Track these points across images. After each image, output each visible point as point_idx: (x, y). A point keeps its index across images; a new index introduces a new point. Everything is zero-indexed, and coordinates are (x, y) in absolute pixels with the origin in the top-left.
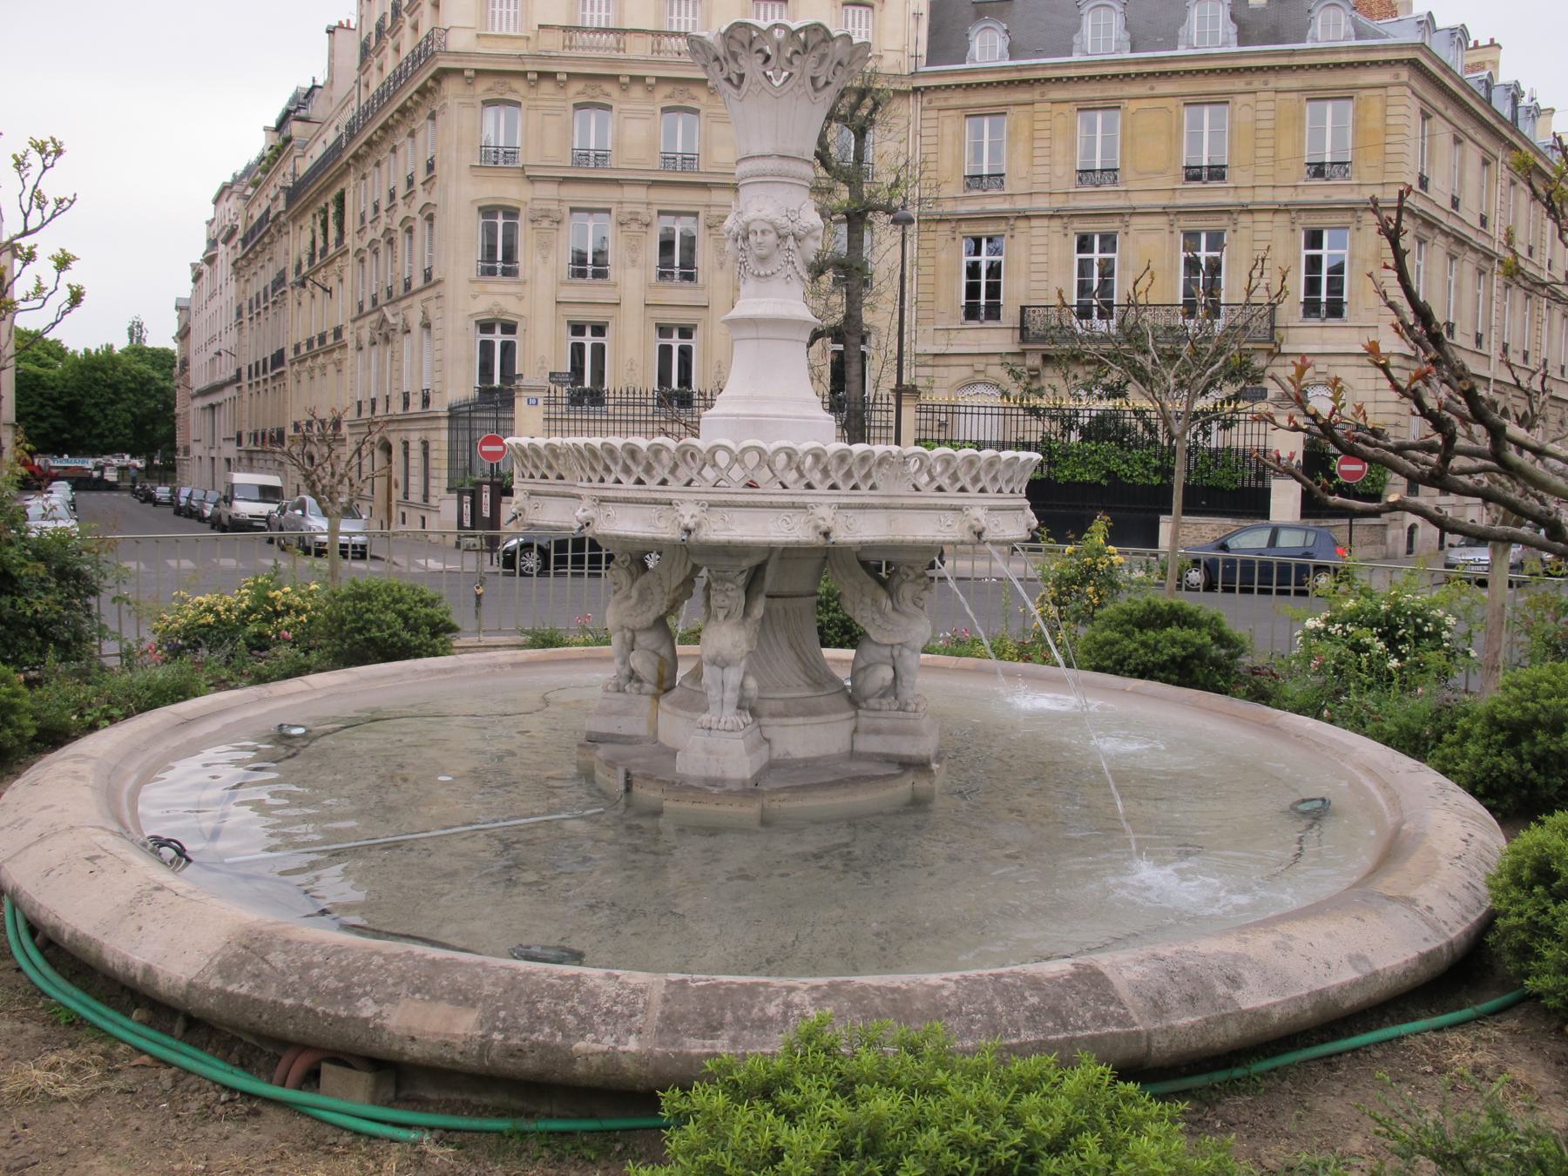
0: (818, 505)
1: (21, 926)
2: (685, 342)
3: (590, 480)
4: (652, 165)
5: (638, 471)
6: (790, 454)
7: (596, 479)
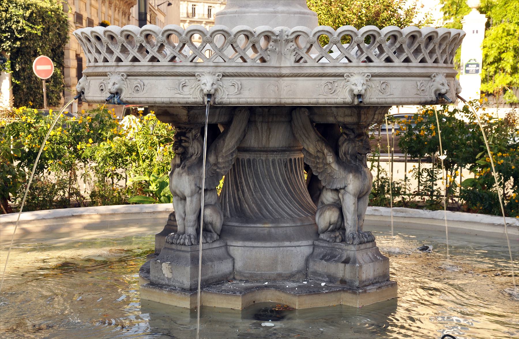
0: (351, 75)
1: (303, 165)
3: (96, 61)
4: (383, 288)
5: (134, 52)
6: (248, 35)
7: (100, 58)
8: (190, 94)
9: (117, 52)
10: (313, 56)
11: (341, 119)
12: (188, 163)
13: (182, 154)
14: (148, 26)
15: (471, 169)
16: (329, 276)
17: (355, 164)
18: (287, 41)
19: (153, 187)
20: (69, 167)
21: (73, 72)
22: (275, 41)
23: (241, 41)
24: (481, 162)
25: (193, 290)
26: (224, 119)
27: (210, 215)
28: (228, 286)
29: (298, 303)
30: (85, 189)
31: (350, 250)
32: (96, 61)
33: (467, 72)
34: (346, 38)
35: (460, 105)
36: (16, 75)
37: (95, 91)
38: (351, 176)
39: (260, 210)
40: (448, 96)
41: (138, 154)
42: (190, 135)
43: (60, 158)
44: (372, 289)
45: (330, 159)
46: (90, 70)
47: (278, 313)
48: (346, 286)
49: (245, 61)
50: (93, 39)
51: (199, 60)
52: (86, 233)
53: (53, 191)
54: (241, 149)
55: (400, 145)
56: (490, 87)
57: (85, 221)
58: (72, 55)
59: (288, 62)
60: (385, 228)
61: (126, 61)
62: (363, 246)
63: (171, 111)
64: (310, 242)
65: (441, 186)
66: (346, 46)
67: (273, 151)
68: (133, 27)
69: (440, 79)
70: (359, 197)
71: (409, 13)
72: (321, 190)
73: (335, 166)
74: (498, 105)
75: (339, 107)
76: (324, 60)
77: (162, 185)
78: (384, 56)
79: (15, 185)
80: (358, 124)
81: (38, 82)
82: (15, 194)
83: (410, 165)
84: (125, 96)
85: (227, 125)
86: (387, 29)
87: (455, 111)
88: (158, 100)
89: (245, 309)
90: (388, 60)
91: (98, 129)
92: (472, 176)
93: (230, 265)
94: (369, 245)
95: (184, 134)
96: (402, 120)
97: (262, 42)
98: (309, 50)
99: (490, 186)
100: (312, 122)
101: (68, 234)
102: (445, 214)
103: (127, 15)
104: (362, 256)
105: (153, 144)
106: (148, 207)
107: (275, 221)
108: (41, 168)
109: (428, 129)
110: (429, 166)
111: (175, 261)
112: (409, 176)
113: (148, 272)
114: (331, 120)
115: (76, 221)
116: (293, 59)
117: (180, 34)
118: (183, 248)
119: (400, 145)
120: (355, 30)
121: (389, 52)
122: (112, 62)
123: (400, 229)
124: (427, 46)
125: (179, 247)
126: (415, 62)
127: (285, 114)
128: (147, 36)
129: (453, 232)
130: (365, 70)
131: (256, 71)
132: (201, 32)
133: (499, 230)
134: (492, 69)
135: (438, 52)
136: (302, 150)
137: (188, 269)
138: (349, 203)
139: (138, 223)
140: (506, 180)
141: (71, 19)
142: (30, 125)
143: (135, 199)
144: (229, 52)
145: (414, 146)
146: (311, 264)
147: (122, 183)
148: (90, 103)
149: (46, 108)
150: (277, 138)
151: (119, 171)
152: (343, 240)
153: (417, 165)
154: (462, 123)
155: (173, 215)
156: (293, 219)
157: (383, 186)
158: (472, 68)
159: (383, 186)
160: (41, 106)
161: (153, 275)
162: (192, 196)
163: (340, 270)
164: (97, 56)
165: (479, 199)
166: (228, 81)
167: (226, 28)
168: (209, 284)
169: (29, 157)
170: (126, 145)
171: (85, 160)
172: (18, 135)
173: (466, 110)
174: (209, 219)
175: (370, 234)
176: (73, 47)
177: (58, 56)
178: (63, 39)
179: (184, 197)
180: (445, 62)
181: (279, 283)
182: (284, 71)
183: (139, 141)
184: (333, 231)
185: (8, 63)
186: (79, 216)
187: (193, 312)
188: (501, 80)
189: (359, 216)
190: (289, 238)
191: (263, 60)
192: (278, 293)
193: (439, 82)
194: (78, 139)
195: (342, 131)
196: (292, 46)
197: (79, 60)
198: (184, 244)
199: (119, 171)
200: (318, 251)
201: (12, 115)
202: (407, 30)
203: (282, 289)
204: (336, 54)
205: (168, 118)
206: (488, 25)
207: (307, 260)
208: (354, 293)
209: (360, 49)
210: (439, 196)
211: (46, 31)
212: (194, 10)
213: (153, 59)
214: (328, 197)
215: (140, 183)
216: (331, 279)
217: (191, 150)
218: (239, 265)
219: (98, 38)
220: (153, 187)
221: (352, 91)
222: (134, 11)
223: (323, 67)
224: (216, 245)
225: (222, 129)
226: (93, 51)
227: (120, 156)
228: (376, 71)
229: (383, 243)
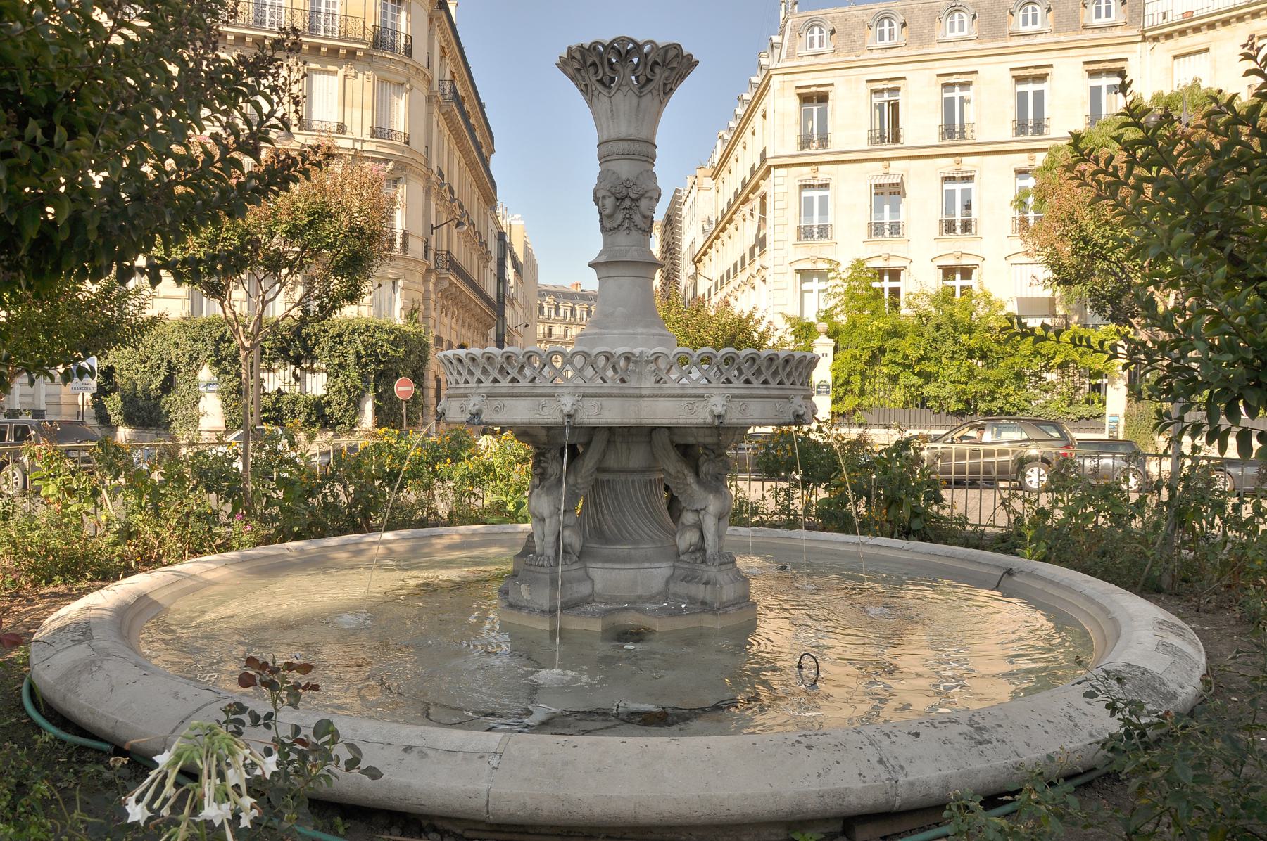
0: (711, 396)
2: (895, 284)
3: (457, 382)
5: (494, 374)
6: (608, 356)
8: (550, 414)
9: (478, 374)
10: (673, 377)
11: (701, 440)
12: (547, 484)
13: (541, 474)
14: (507, 348)
15: (826, 488)
16: (689, 598)
17: (716, 484)
18: (648, 362)
19: (510, 507)
20: (428, 487)
21: (432, 393)
22: (635, 362)
23: (601, 361)
24: (835, 481)
25: (552, 612)
26: (583, 439)
27: (568, 536)
28: (588, 608)
29: (658, 625)
30: (443, 509)
31: (711, 572)
32: (457, 382)
33: (819, 393)
34: (707, 359)
35: (814, 425)
36: (378, 396)
37: (455, 412)
38: (711, 497)
39: (620, 531)
40: (805, 417)
41: (495, 474)
42: (548, 455)
43: (419, 477)
44: (732, 610)
45: (691, 479)
46: (451, 392)
47: (637, 635)
48: (706, 607)
49: (605, 382)
50: (454, 362)
51: (558, 380)
52: (452, 556)
53: (412, 512)
54: (600, 470)
55: (758, 465)
56: (841, 408)
57: (446, 541)
58: (432, 376)
59: (648, 383)
60: (746, 550)
61: (487, 383)
62: (723, 567)
63: (530, 431)
64: (670, 564)
65: (797, 505)
66: (706, 367)
67: (633, 471)
68: (492, 349)
69: (798, 401)
70: (720, 518)
71: (763, 336)
72: (681, 512)
73: (695, 487)
74: (850, 425)
75: (698, 427)
76: (684, 381)
77: (519, 505)
78: (743, 378)
79: (376, 505)
80: (718, 444)
81: (398, 403)
82: (376, 513)
83: (768, 485)
84: (485, 417)
85: (587, 445)
86: (746, 352)
87: (810, 430)
88: (518, 421)
89: (605, 631)
90: (747, 381)
91: (457, 447)
92: (827, 495)
93: (590, 587)
94: (730, 566)
95: (543, 455)
96: (760, 439)
97: (622, 362)
98: (669, 370)
99: (844, 506)
100: (672, 442)
101: (429, 555)
102: (803, 533)
103: (485, 336)
104: (722, 577)
105: (510, 464)
106: (508, 528)
107: (635, 542)
108: (401, 488)
109: (784, 448)
110: (785, 485)
111: (533, 582)
112: (767, 495)
113: (507, 593)
114: (691, 440)
115: (435, 541)
116: (653, 379)
117: (540, 356)
118: (542, 570)
119: (758, 465)
120: (690, 350)
121: (748, 374)
122: (473, 384)
123: (757, 550)
124: (784, 369)
125: (538, 569)
126: (773, 384)
127: (648, 433)
128: (508, 357)
129: (810, 551)
130: (725, 391)
131: (616, 391)
132: (563, 354)
133: (853, 549)
134: (841, 391)
135: (795, 374)
136: (662, 470)
137: (547, 591)
138: (710, 524)
139: (499, 543)
140: (859, 499)
141: (432, 341)
142: (391, 445)
143: (494, 519)
144: (589, 372)
145: (770, 467)
146: (671, 585)
147: (479, 502)
148: (448, 424)
149: (405, 428)
150: (637, 457)
151: (476, 491)
152: (704, 562)
153: (773, 484)
154: (816, 442)
155: (531, 536)
156: (653, 541)
157: (741, 506)
158: (823, 389)
159: (741, 506)
160: (401, 426)
161: (511, 598)
162: (551, 517)
163: (700, 592)
164: (458, 377)
165: (833, 518)
166: (588, 402)
167: (586, 350)
168: (568, 606)
169: (390, 478)
170: (483, 464)
171: (443, 481)
172: (379, 457)
173: (820, 430)
174: (568, 541)
175: (730, 555)
176: (434, 366)
177: (418, 377)
178: (424, 360)
179: (541, 517)
180: (802, 384)
181: (639, 605)
182: (644, 392)
183: (497, 461)
184: (693, 552)
185: (372, 386)
186: (440, 536)
187: (553, 634)
188: (850, 402)
189: (720, 537)
190: (648, 560)
191: (623, 381)
192: (637, 615)
193: (797, 404)
194: (437, 459)
195: (699, 453)
196: (652, 367)
197: (438, 381)
198: (543, 566)
199: (476, 491)
200: (678, 572)
201: (375, 435)
202: (764, 352)
203: (643, 611)
204: (695, 374)
205: (527, 439)
206: (836, 349)
207: (667, 582)
208: (715, 614)
209: (719, 369)
210: (796, 514)
211: (408, 353)
212: (550, 330)
213: (514, 380)
214: (688, 518)
215: (497, 503)
216: (692, 600)
217: (550, 471)
218: (598, 587)
219: (460, 361)
220: (510, 507)
221: (712, 411)
222: (492, 333)
223: (683, 387)
224: (575, 566)
225: (581, 450)
226: (455, 373)
227: (477, 475)
228: (736, 392)
229: (745, 562)
